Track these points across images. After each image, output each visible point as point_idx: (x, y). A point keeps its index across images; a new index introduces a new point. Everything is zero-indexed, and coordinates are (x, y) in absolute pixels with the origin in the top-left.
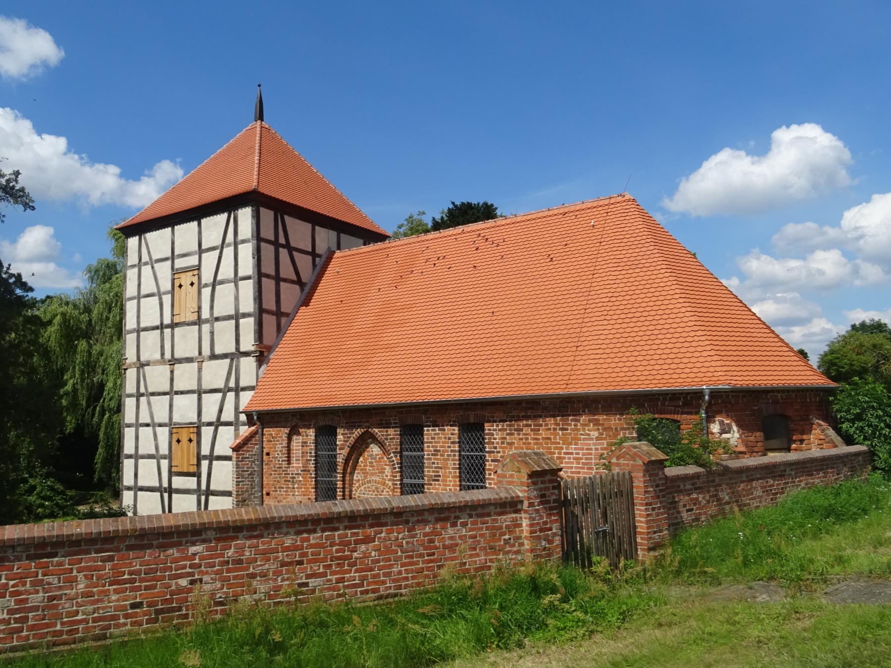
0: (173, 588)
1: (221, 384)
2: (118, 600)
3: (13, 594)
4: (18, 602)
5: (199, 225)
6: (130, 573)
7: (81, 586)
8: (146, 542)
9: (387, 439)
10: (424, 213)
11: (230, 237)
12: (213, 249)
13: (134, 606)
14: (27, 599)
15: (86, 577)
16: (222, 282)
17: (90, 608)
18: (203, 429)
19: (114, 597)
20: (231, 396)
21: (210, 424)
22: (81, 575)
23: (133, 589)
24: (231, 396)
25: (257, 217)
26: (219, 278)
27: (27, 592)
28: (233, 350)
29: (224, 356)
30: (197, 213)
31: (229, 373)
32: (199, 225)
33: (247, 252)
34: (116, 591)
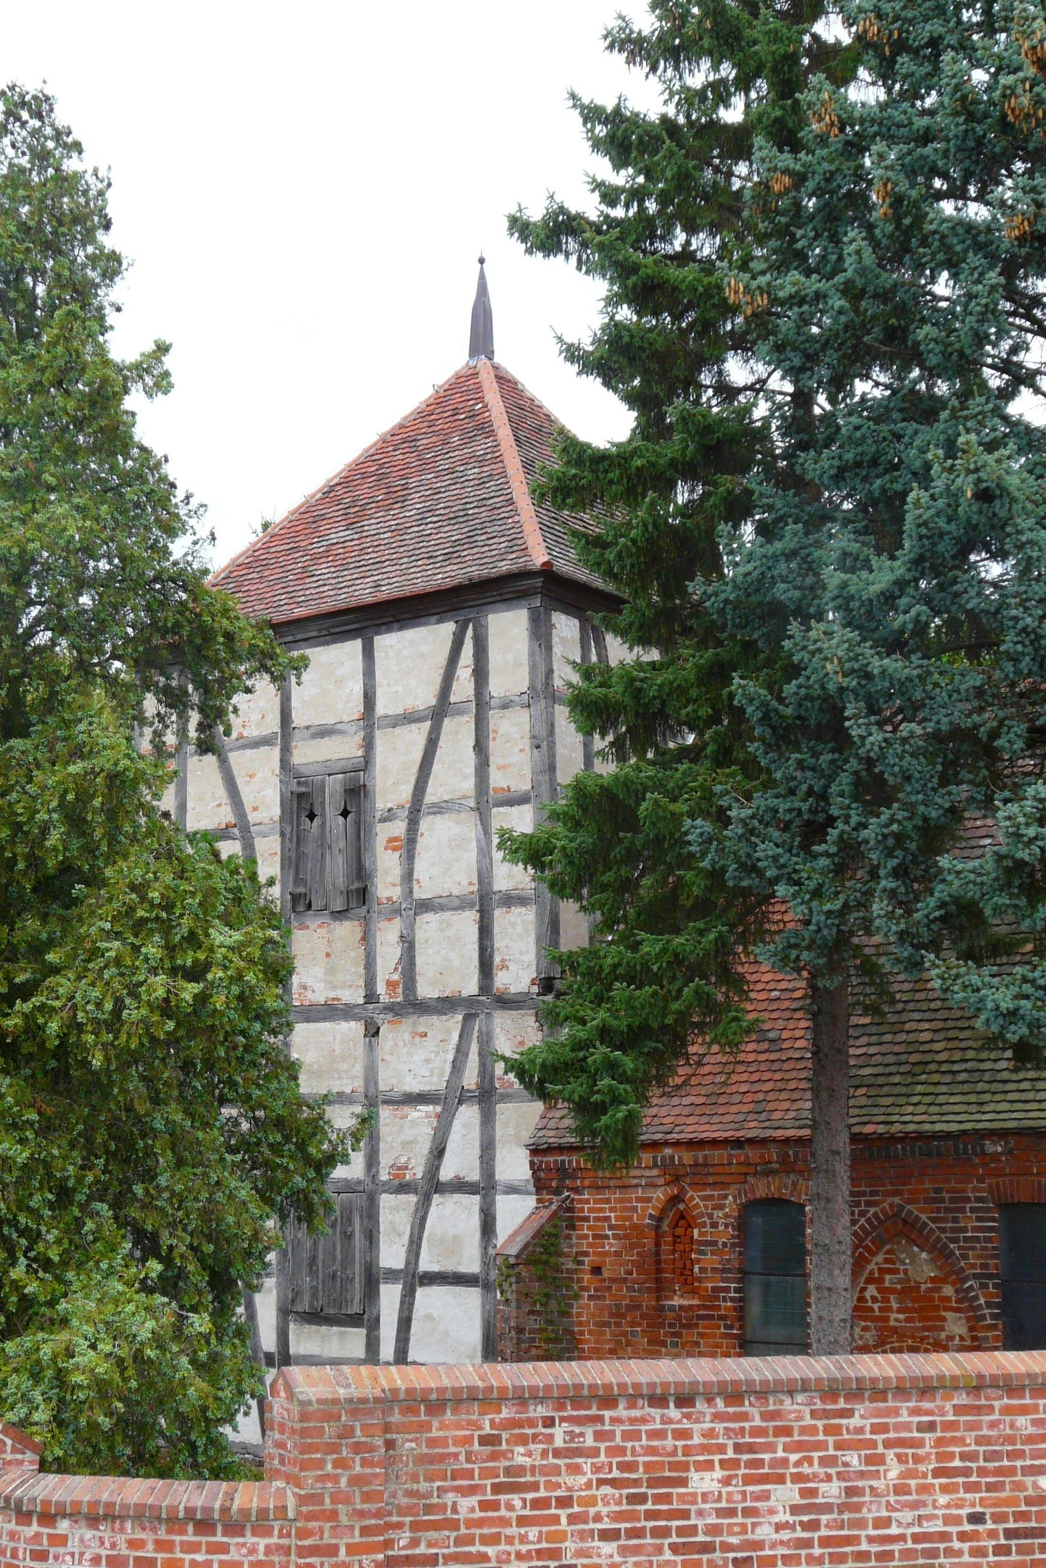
0: (1030, 1492)
1: (437, 1083)
2: (948, 1506)
3: (798, 1478)
4: (805, 1493)
5: (368, 652)
6: (963, 1457)
7: (893, 1474)
8: (983, 1402)
9: (955, 1240)
10: (119, 309)
11: (463, 687)
12: (409, 718)
13: (976, 1518)
14: (816, 1489)
15: (899, 1457)
16: (440, 809)
17: (907, 1516)
18: (386, 1201)
19: (943, 1499)
20: (468, 1116)
21: (403, 1188)
22: (890, 1454)
23: (970, 1488)
24: (468, 1116)
25: (541, 633)
26: (431, 796)
27: (815, 1477)
28: (471, 987)
29: (446, 1005)
30: (365, 620)
31: (461, 1052)
32: (368, 652)
33: (512, 731)
34: (945, 1489)
